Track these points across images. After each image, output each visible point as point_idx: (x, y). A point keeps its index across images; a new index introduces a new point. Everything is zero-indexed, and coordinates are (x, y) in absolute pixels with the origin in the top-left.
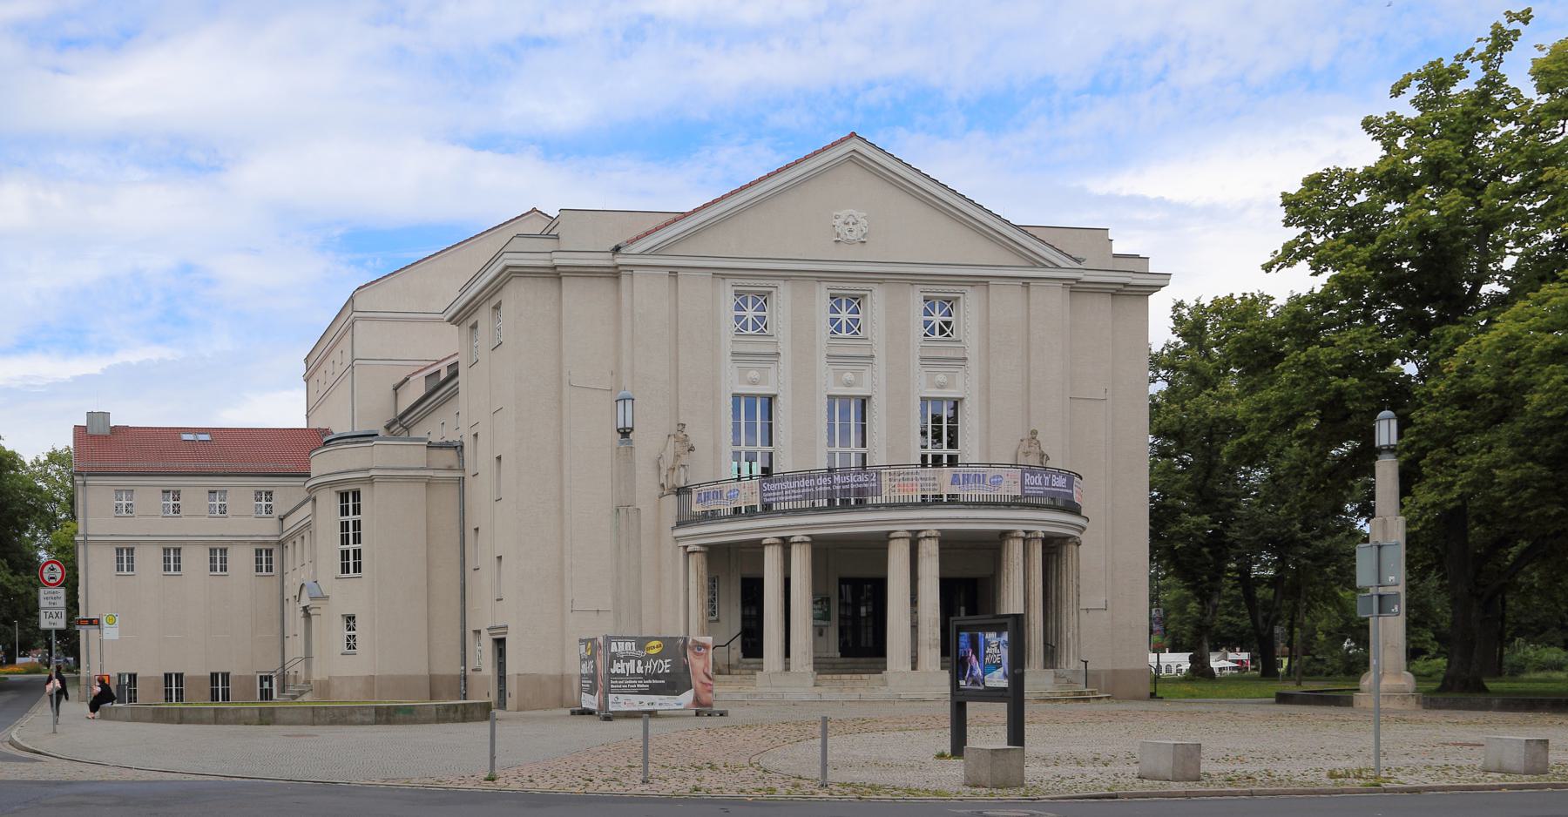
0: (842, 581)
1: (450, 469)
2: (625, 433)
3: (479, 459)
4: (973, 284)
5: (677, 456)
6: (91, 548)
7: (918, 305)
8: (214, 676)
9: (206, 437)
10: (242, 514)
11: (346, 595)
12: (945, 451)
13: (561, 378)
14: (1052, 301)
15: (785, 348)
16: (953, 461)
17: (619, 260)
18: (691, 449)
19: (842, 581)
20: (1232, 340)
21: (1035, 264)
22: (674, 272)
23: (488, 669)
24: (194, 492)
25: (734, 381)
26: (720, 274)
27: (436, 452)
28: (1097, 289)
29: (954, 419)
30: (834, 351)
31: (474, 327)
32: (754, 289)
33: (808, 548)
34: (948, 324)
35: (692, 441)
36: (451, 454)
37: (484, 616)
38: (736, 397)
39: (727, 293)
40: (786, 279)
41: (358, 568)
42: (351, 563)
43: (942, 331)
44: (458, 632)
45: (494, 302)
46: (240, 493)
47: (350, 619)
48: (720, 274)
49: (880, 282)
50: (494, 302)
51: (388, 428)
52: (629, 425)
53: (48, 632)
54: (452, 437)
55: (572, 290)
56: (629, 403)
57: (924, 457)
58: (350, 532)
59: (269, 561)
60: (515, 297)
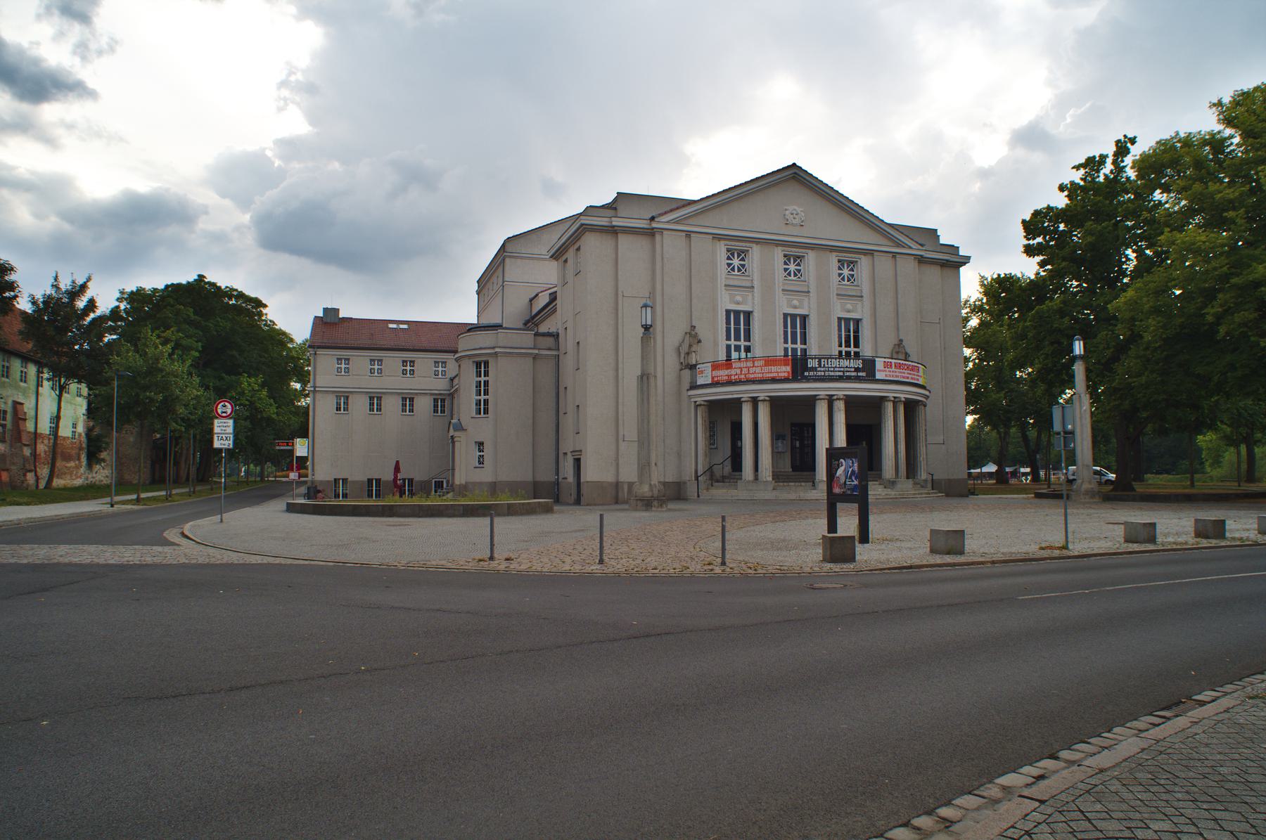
0: (793, 425)
1: (550, 349)
2: (647, 328)
3: (568, 343)
4: (865, 254)
5: (690, 346)
6: (318, 396)
7: (835, 264)
8: (370, 481)
9: (405, 326)
10: (427, 376)
11: (481, 429)
12: (852, 349)
13: (617, 294)
14: (908, 267)
15: (756, 284)
16: (857, 354)
17: (654, 225)
18: (699, 341)
19: (793, 425)
20: (1003, 291)
21: (899, 245)
22: (688, 234)
23: (571, 479)
24: (393, 361)
25: (726, 302)
26: (718, 238)
27: (540, 338)
28: (933, 262)
29: (856, 331)
30: (731, 283)
31: (566, 261)
32: (738, 249)
33: (768, 404)
34: (743, 266)
35: (701, 336)
36: (551, 339)
37: (567, 446)
38: (785, 315)
39: (721, 249)
40: (757, 243)
41: (486, 411)
42: (483, 408)
43: (739, 270)
44: (554, 454)
45: (576, 246)
46: (424, 363)
47: (480, 444)
48: (718, 238)
49: (812, 249)
50: (576, 246)
51: (525, 324)
52: (649, 322)
53: (220, 450)
54: (553, 330)
55: (622, 238)
56: (649, 310)
57: (840, 352)
58: (483, 388)
59: (443, 406)
60: (591, 243)
